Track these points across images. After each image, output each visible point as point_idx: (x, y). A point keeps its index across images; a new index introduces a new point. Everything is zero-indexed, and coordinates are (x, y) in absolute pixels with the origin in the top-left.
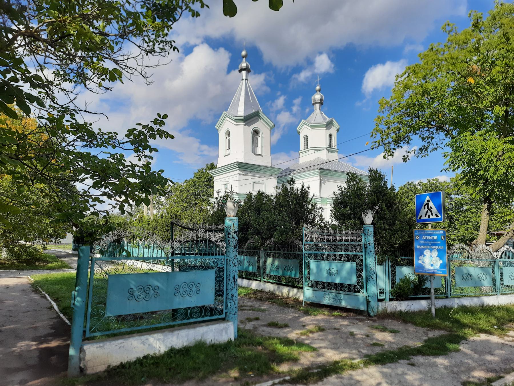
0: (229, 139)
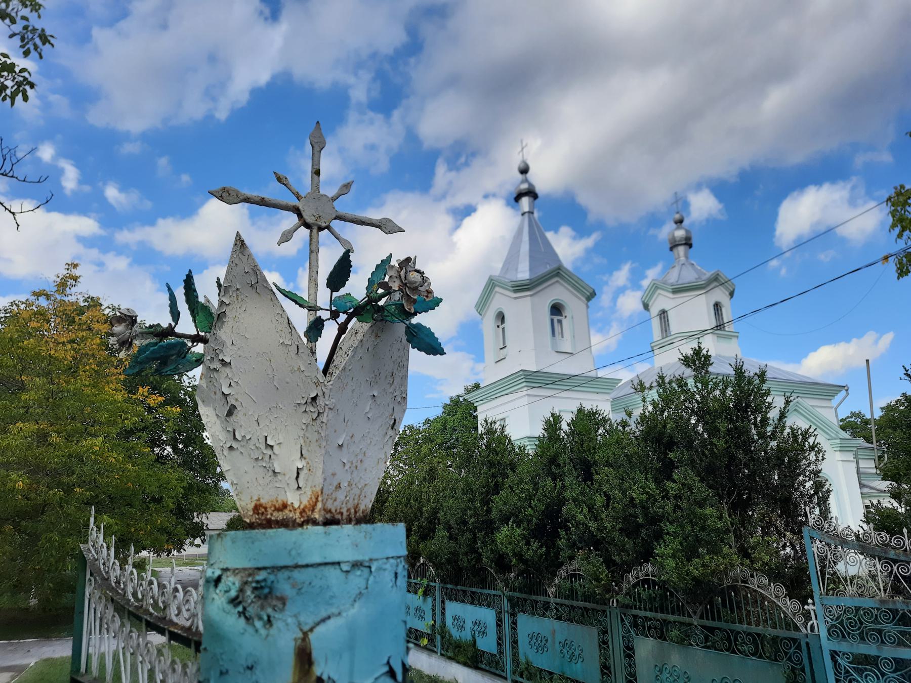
0: (503, 329)
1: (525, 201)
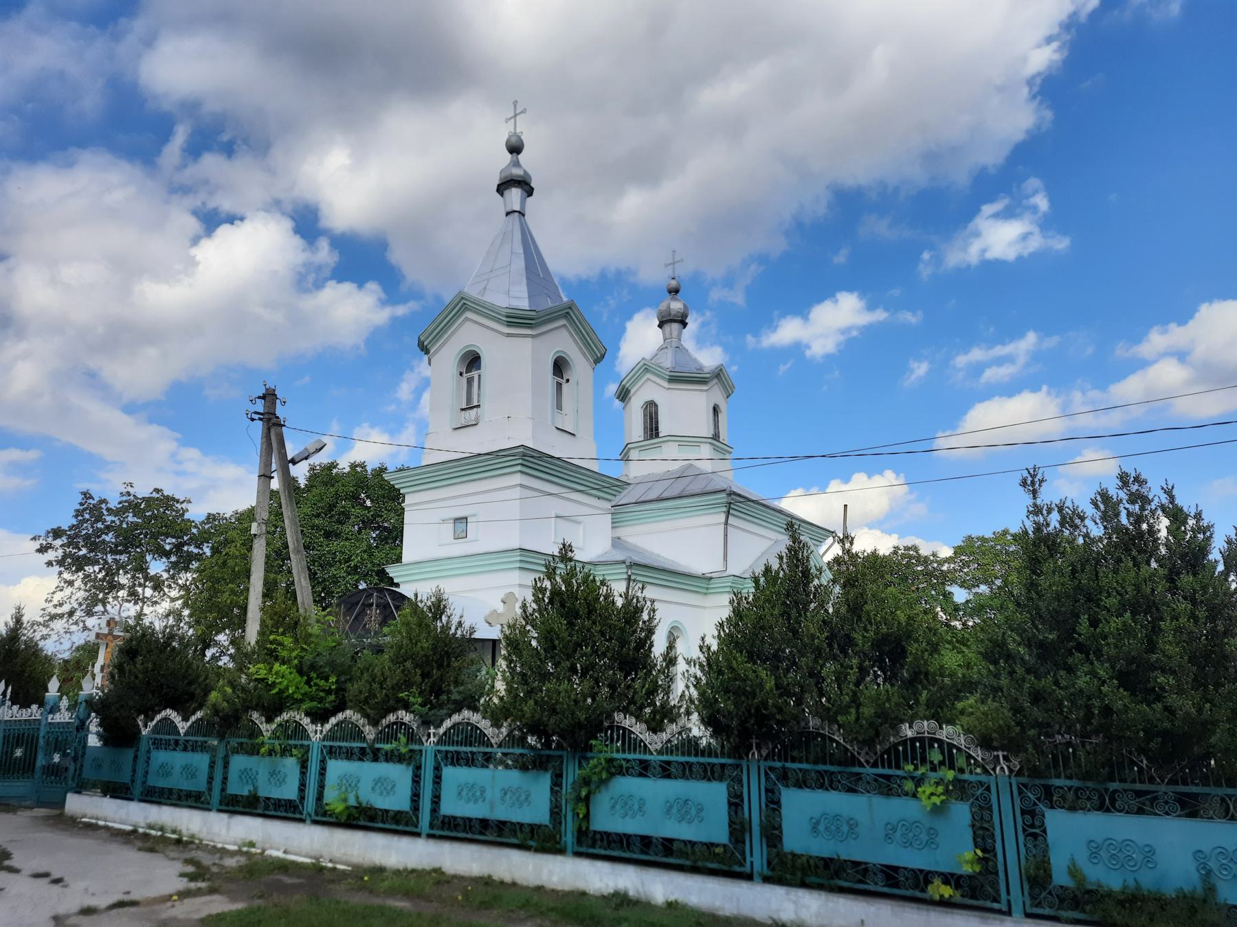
1: (515, 194)
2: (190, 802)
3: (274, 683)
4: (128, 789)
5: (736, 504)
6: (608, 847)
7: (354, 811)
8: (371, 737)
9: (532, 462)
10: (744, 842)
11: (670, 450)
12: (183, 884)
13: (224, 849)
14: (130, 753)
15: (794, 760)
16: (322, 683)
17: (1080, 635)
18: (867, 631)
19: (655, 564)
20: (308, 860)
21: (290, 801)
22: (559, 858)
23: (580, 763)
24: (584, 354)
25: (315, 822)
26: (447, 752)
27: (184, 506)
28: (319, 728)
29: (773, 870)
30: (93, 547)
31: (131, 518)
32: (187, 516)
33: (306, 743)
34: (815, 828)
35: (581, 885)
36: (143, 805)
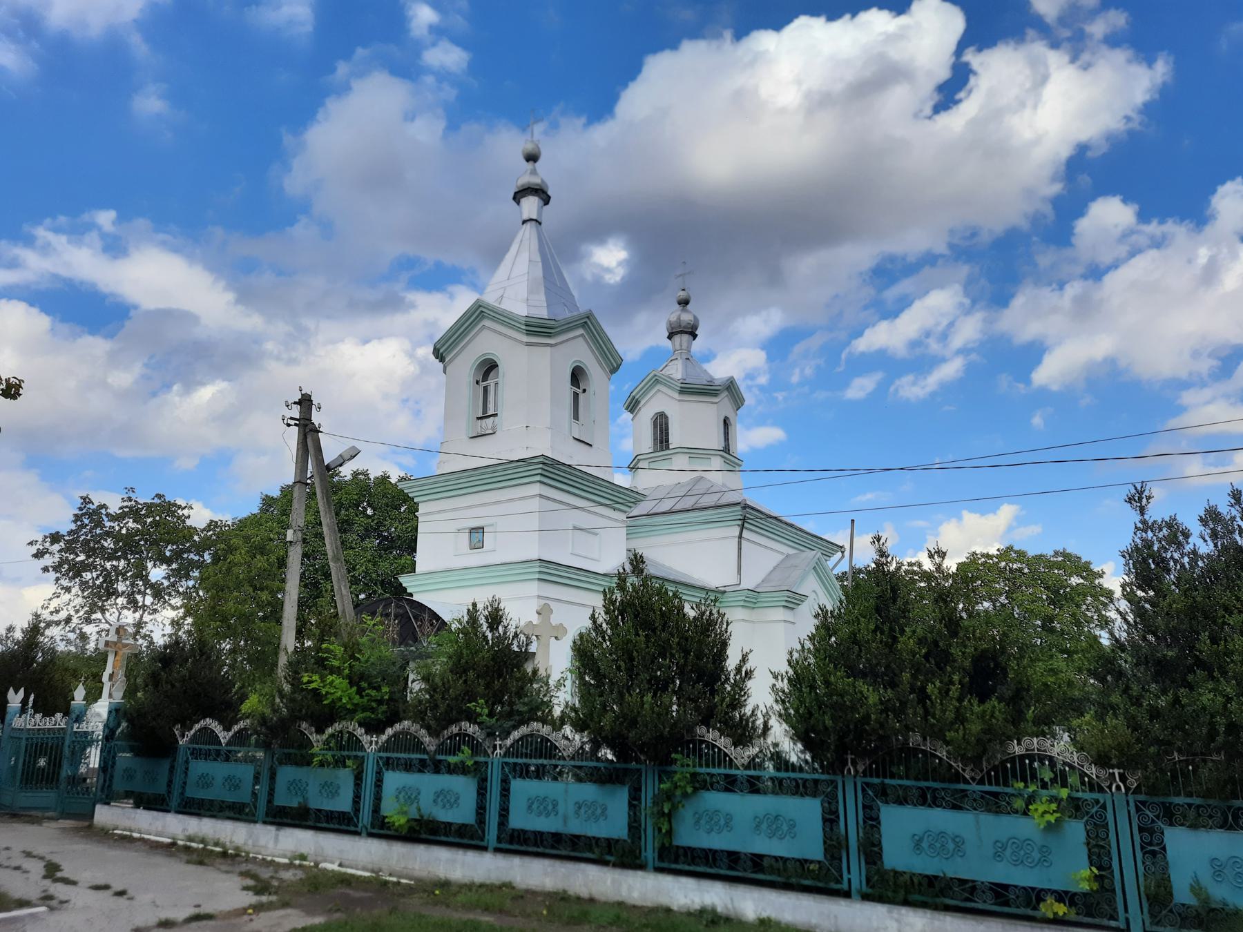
2: (227, 813)
3: (327, 693)
4: (164, 800)
5: (749, 518)
6: (693, 861)
7: (414, 824)
8: (433, 748)
9: (552, 471)
10: (840, 859)
11: (680, 461)
12: (250, 898)
13: (273, 861)
14: (166, 765)
15: (892, 776)
16: (373, 693)
17: (1201, 652)
18: (965, 647)
19: (683, 580)
20: (367, 874)
21: (344, 813)
22: (640, 873)
23: (660, 777)
24: (600, 364)
25: (371, 835)
26: (515, 764)
27: (186, 512)
28: (374, 739)
29: (872, 887)
30: (90, 552)
31: (131, 525)
32: (188, 523)
33: (360, 754)
34: (918, 845)
35: (664, 900)
36: (180, 816)
